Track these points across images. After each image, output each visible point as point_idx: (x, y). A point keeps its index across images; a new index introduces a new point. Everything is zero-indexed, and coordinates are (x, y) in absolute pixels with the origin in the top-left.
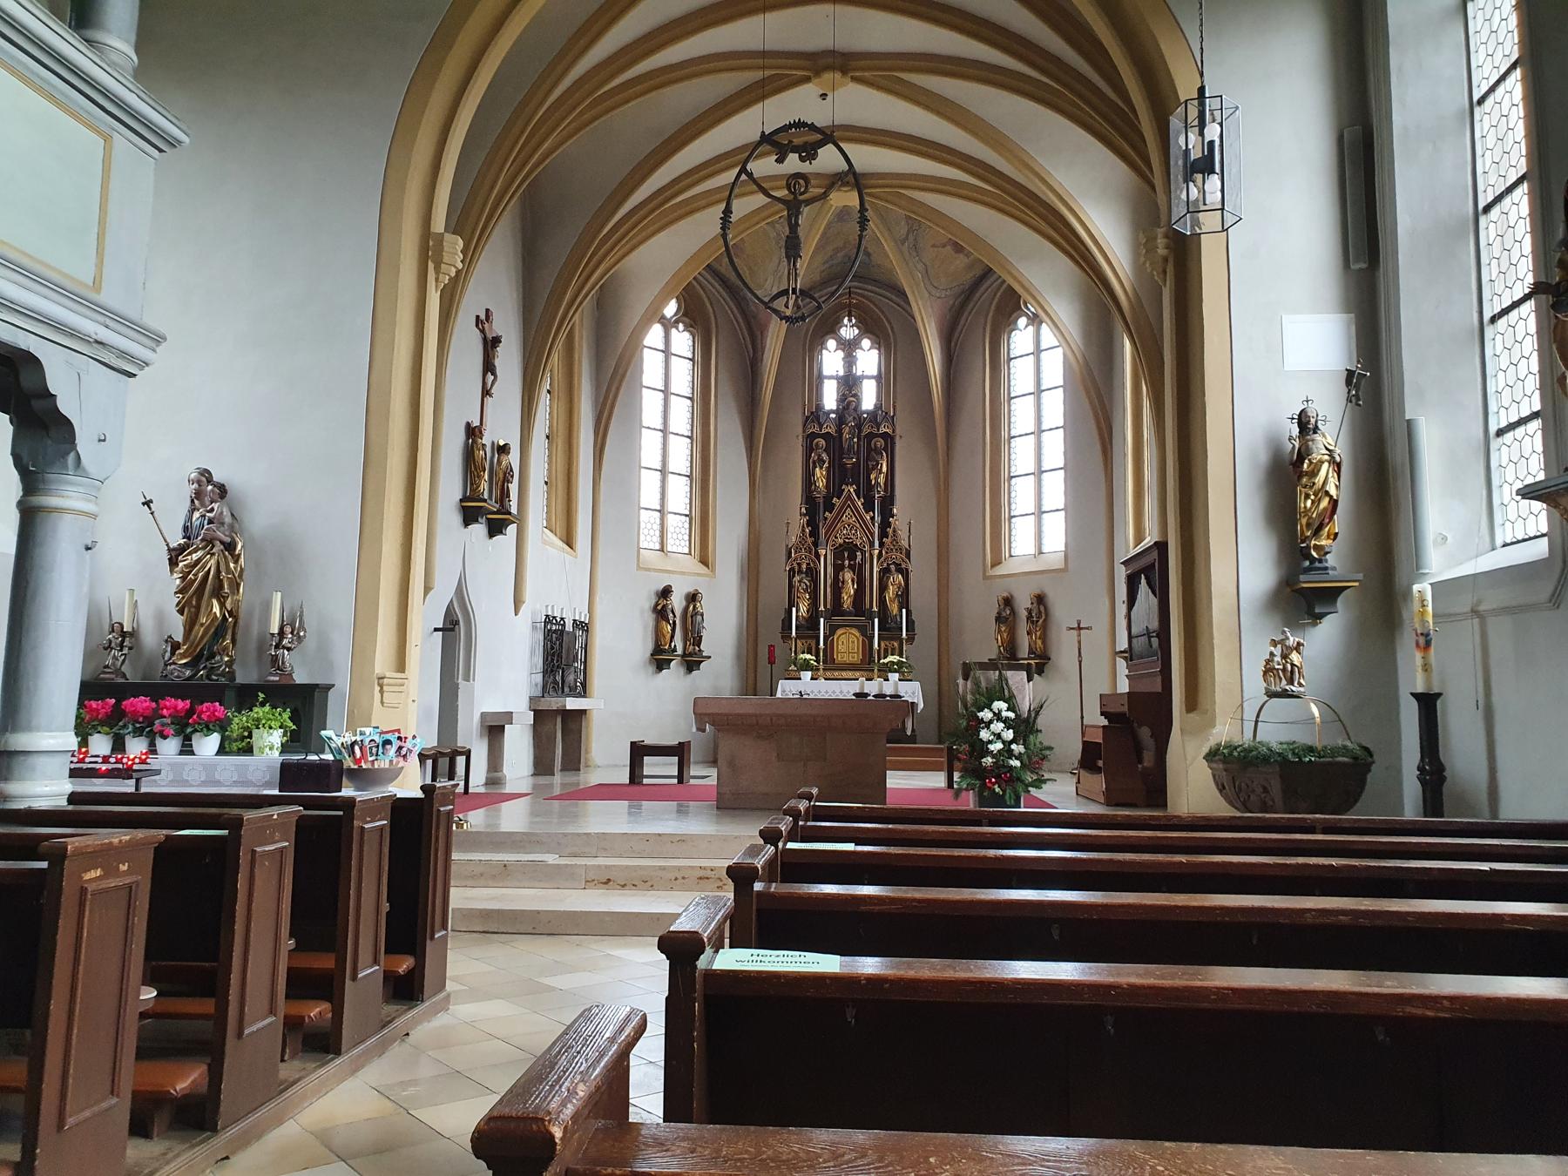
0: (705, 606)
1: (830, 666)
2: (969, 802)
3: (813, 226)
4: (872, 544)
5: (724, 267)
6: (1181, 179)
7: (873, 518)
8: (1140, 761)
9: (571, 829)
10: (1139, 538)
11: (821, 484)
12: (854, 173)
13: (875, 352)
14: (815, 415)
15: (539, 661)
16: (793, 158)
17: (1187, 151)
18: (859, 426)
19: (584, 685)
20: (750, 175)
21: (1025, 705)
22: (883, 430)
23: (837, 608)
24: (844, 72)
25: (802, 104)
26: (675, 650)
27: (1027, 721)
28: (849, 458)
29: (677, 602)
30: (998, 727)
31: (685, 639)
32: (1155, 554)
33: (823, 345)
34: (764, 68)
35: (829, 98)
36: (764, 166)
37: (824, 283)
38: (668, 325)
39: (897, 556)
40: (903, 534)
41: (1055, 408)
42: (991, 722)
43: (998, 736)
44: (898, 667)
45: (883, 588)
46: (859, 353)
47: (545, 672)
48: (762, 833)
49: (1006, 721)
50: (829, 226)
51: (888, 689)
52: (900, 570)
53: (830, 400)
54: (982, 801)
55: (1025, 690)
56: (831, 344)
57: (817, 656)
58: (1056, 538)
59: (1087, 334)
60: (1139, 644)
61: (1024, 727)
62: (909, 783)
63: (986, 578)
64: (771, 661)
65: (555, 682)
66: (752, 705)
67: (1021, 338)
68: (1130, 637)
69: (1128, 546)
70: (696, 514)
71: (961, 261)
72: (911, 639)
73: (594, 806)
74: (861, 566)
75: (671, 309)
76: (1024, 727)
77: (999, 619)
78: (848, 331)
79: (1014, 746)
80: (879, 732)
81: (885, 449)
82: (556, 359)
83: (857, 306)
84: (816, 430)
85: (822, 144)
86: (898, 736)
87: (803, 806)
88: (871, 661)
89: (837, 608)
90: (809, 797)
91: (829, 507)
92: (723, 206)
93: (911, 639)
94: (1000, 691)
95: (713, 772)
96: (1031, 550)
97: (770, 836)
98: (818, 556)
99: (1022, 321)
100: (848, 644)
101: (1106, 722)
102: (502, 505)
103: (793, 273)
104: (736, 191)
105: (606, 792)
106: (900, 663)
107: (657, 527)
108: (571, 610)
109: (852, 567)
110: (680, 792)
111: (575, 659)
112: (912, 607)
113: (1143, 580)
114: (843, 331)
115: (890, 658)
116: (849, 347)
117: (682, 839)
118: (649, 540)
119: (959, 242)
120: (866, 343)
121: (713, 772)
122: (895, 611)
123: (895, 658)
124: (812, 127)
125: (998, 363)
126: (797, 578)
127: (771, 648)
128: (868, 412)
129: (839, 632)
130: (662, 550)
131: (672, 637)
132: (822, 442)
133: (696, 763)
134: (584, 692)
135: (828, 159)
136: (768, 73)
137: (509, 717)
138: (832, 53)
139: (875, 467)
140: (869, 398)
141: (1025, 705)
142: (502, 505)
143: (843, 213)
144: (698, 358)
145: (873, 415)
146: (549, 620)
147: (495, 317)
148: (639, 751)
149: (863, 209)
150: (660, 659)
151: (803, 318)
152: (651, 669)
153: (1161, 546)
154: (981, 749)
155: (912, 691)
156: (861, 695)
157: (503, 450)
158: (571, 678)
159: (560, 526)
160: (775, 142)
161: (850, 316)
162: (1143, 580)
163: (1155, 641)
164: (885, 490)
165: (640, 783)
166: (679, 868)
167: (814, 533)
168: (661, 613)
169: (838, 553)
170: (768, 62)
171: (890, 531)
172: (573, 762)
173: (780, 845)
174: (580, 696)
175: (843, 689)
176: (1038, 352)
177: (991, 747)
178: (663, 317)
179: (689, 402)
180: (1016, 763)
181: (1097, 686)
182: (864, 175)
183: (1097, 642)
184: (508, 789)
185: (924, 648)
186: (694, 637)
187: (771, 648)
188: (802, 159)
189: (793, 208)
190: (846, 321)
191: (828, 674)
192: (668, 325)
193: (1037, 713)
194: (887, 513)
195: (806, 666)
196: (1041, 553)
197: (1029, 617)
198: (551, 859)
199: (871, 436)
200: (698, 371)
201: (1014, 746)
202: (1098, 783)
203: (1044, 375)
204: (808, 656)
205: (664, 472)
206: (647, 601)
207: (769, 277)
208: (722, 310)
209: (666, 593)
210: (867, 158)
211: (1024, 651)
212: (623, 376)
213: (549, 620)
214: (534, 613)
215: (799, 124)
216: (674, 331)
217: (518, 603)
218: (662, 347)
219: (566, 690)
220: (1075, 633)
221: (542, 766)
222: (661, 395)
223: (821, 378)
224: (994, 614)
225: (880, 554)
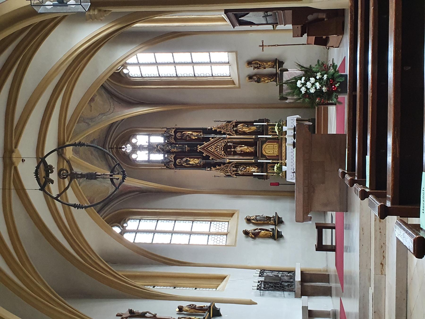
0: (252, 215)
1: (280, 157)
2: (345, 98)
3: (81, 166)
4: (224, 138)
5: (99, 206)
6: (65, 7)
7: (213, 138)
8: (324, 19)
9: (358, 281)
10: (223, 20)
11: (197, 161)
12: (59, 148)
13: (138, 137)
14: (166, 164)
15: (278, 293)
16: (51, 176)
17: (53, 5)
18: (171, 144)
19: (289, 272)
20: (59, 196)
21: (298, 72)
22: (173, 133)
23: (254, 154)
24: (12, 152)
25: (27, 171)
26: (273, 229)
27: (306, 72)
28: (184, 149)
29: (250, 228)
30: (309, 85)
31: (268, 224)
32: (230, 14)
33: (134, 160)
34: (10, 189)
35: (24, 159)
36: (54, 190)
37: (106, 160)
38: (124, 231)
39: (230, 126)
40: (220, 124)
41: (164, 57)
42: (306, 88)
43: (313, 84)
44: (280, 126)
45: (244, 133)
46: (138, 144)
47: (284, 291)
48: (362, 198)
49: (306, 81)
50: (82, 158)
51: (290, 133)
52: (236, 126)
53: (159, 157)
54: (344, 91)
55: (292, 72)
56: (134, 156)
57: (275, 163)
58: (222, 56)
59: (132, 42)
60: (270, 20)
61: (309, 73)
62: (334, 121)
63: (239, 87)
64: (278, 184)
65: (288, 286)
66: (299, 195)
67: (133, 72)
68: (267, 24)
69: (226, 25)
70: (210, 219)
71: (98, 99)
72: (267, 121)
73: (346, 268)
74: (234, 143)
75: (117, 230)
76: (309, 73)
77: (258, 81)
78: (128, 148)
79: (318, 78)
80: (310, 135)
81: (182, 132)
82: (139, 283)
83: (117, 146)
84: (172, 163)
85: (45, 163)
86: (312, 129)
87: (348, 177)
88: (277, 139)
89: (254, 154)
90: (344, 174)
91: (207, 157)
92: (72, 208)
93: (267, 121)
94: (293, 83)
95: (329, 213)
96: (227, 67)
97: (364, 195)
98: (229, 163)
99: (125, 71)
100: (269, 149)
101: (306, 35)
102: (206, 310)
103: (103, 176)
104: (65, 201)
105: (339, 263)
106: (278, 126)
107: (216, 237)
108: (254, 278)
109: (234, 148)
110: (339, 228)
111: (277, 276)
112: (253, 120)
113: (242, 18)
114: (128, 151)
115: (276, 130)
116: (136, 148)
117: (362, 229)
118: (222, 241)
119: (89, 99)
120: (134, 141)
121: (329, 213)
122: (255, 128)
123: (276, 128)
124: (38, 167)
125: (144, 82)
126: (240, 172)
127: (272, 184)
128: (165, 140)
129: (264, 153)
130: (227, 235)
131: (267, 230)
132: (178, 160)
133: (325, 219)
134: (292, 272)
135: (51, 160)
136: (12, 187)
137: (304, 308)
138: (4, 158)
139: (190, 137)
140: (159, 139)
141: (298, 72)
142: (206, 310)
143: (76, 152)
144: (139, 217)
145: (166, 138)
146: (259, 288)
147: (120, 312)
148: (320, 247)
149: (74, 145)
150: (277, 236)
151: (123, 172)
152: (281, 240)
153: (226, 12)
154: (319, 92)
155: (292, 121)
156: (294, 145)
157: (181, 309)
158: (286, 278)
159: (215, 282)
160: (44, 185)
161: (121, 148)
162: (242, 18)
163: (269, 13)
164: (200, 132)
165: (335, 246)
166: (376, 231)
167: (219, 164)
168: (256, 235)
169: (228, 153)
170: (7, 187)
171: (218, 130)
172: (325, 278)
173: (367, 190)
174: (294, 274)
175: (291, 154)
176: (138, 64)
177: (318, 87)
178: (121, 233)
179: (159, 221)
180: (325, 77)
181: (289, 37)
182: (58, 145)
183: (271, 38)
184: (338, 308)
185: (272, 115)
186: (267, 220)
187: (272, 184)
188: (52, 172)
189: (73, 176)
190: (124, 150)
191: (283, 158)
192: (124, 231)
193: (302, 67)
194: (210, 131)
195: (280, 168)
196: (228, 63)
197: (258, 68)
198: (371, 291)
199: (175, 138)
200: (145, 217)
201: (318, 78)
202: (333, 38)
203: (149, 61)
204: (275, 167)
205: (191, 233)
206: (250, 242)
207: (105, 187)
208: (116, 208)
209: (246, 233)
210: (51, 143)
211: (273, 70)
212: (148, 252)
213: (259, 288)
214: (256, 295)
215: (37, 173)
216: (127, 228)
217: (251, 303)
218: (134, 234)
219: (291, 280)
220: (264, 48)
221: (327, 292)
222: (156, 235)
223: (149, 161)
224: (256, 83)
225: (229, 134)
